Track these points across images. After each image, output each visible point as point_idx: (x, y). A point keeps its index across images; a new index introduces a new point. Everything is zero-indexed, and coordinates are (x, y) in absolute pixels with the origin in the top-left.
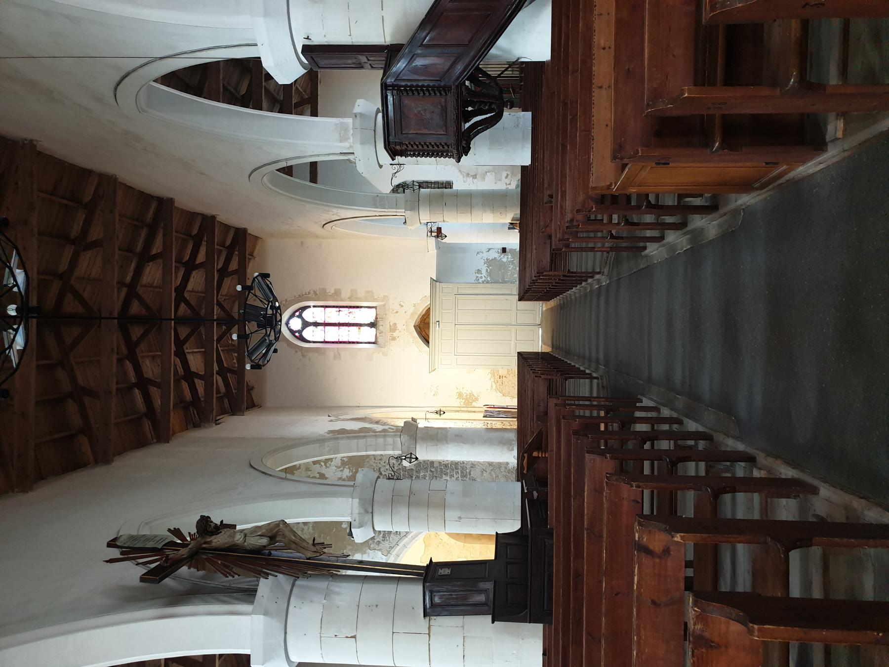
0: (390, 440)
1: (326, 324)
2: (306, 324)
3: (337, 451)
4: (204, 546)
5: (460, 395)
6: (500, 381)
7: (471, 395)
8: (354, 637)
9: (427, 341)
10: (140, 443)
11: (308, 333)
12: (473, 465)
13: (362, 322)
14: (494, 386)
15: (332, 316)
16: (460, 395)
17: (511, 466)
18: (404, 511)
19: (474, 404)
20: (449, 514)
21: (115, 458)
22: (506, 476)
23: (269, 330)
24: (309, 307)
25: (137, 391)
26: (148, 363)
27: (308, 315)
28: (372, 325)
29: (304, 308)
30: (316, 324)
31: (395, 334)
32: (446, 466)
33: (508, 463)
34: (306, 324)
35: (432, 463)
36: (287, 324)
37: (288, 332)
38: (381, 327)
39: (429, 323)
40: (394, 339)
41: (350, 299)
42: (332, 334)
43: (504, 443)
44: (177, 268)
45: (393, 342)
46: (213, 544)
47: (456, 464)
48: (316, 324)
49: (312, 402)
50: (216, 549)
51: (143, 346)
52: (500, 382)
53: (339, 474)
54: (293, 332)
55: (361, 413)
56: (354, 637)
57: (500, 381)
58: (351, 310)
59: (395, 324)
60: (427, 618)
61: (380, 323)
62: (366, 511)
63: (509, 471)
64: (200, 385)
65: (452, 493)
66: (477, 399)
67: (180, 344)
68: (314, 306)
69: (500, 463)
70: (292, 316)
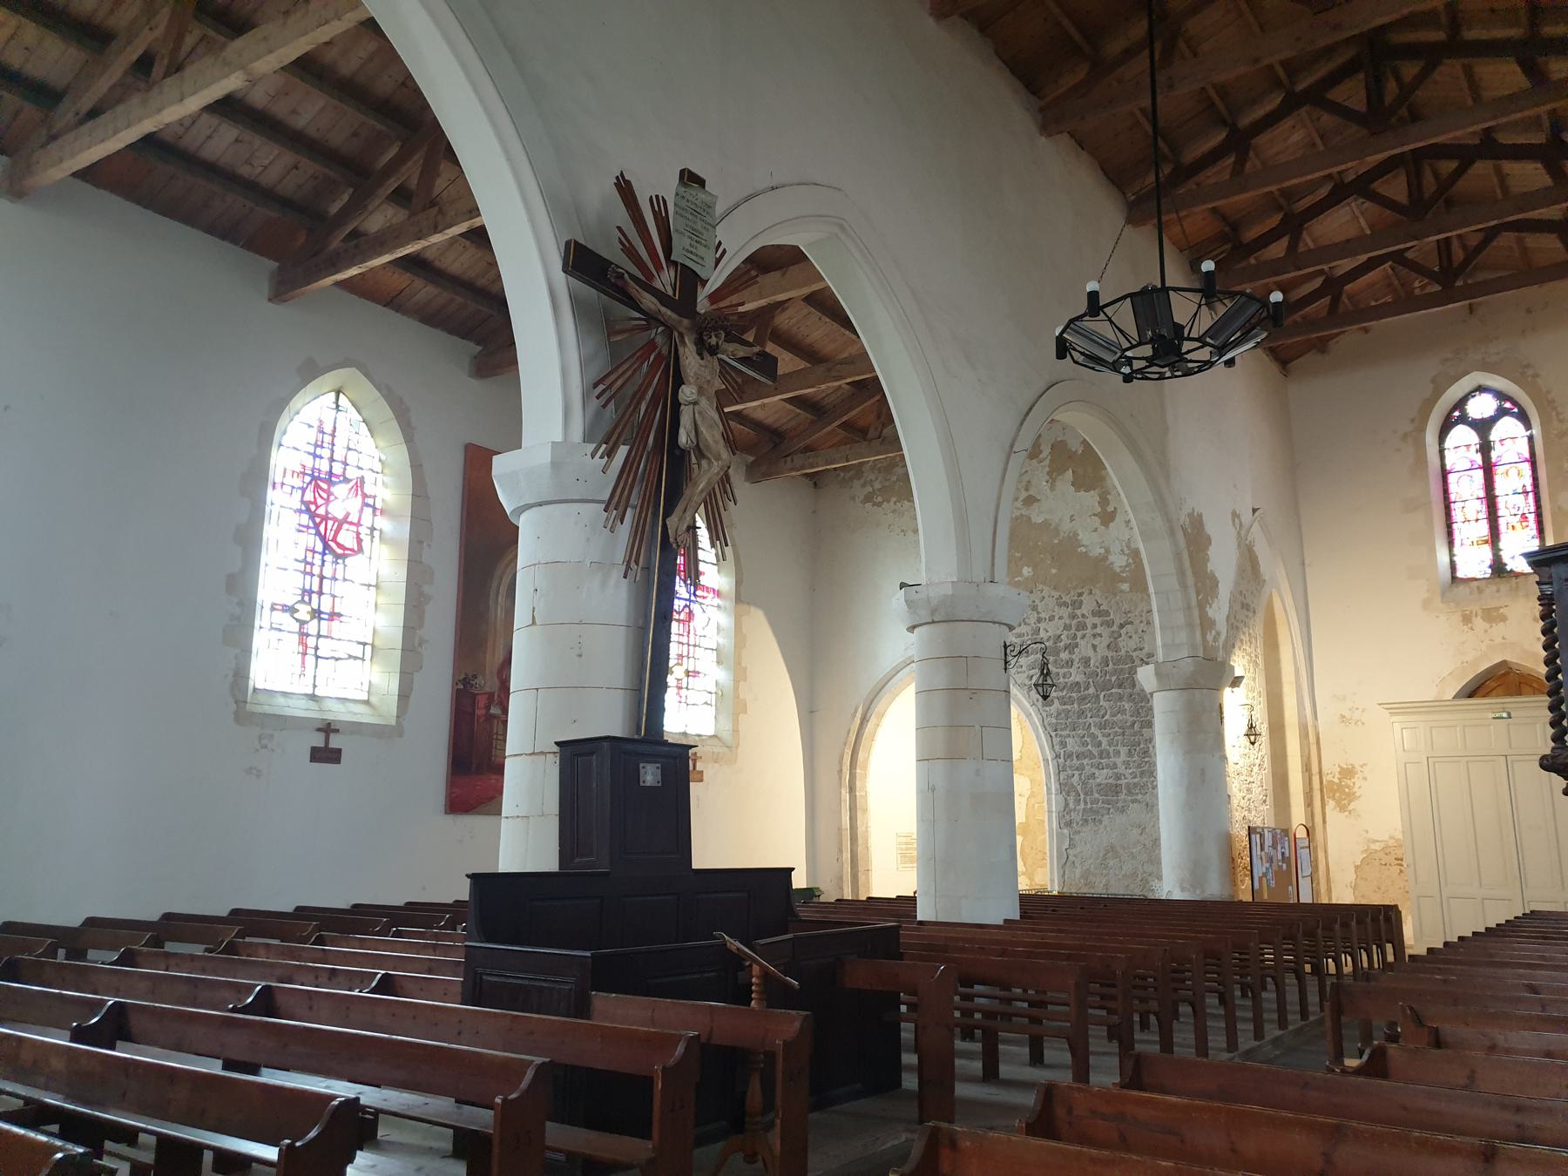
0: (1183, 636)
1: (1488, 469)
2: (1482, 427)
3: (1146, 537)
4: (676, 334)
5: (1348, 772)
6: (1390, 859)
7: (1351, 797)
8: (534, 623)
9: (1475, 690)
10: (1116, 176)
11: (1462, 436)
12: (1151, 807)
13: (1501, 545)
14: (1377, 847)
15: (1513, 482)
16: (1348, 772)
17: (1155, 883)
18: (941, 681)
19: (1331, 804)
20: (940, 766)
21: (1065, 138)
22: (1135, 874)
23: (1147, 350)
24: (1528, 426)
25: (1220, 136)
26: (1297, 137)
27: (1508, 427)
28: (1498, 568)
29: (1523, 417)
30: (1485, 448)
31: (1479, 623)
32: (1146, 753)
33: (1160, 878)
34: (1482, 427)
35: (1150, 725)
36: (1481, 389)
37: (1460, 395)
38: (1494, 588)
39: (1520, 694)
40: (1467, 619)
41: (1558, 512)
42: (1466, 488)
43: (1195, 871)
44: (1535, 123)
45: (1457, 618)
46: (681, 349)
47: (1152, 773)
48: (1485, 448)
49: (1298, 468)
50: (677, 358)
51: (1327, 119)
52: (1386, 859)
53: (1115, 548)
54: (1461, 404)
55: (1273, 568)
56: (534, 623)
57: (1390, 859)
58: (1532, 517)
59: (1504, 619)
60: (556, 749)
61: (1504, 586)
62: (934, 611)
63: (1145, 881)
64: (1278, 249)
65: (977, 773)
66: (1343, 809)
67: (1362, 187)
68: (1531, 438)
69: (1159, 863)
70: (1501, 396)
